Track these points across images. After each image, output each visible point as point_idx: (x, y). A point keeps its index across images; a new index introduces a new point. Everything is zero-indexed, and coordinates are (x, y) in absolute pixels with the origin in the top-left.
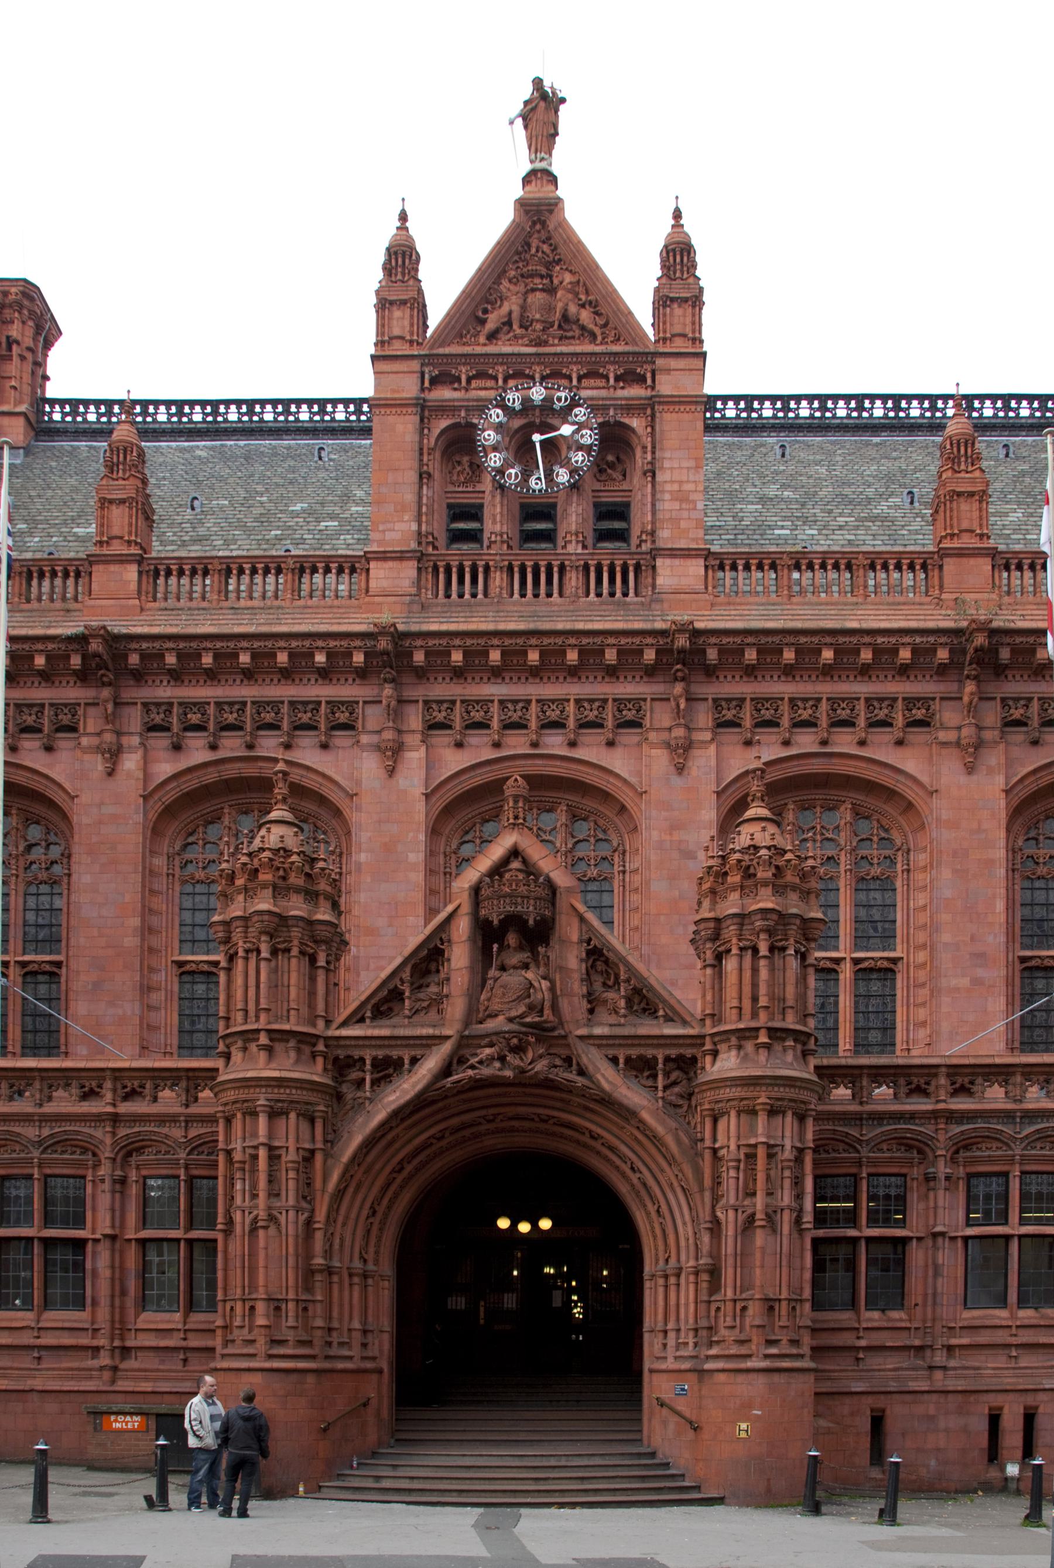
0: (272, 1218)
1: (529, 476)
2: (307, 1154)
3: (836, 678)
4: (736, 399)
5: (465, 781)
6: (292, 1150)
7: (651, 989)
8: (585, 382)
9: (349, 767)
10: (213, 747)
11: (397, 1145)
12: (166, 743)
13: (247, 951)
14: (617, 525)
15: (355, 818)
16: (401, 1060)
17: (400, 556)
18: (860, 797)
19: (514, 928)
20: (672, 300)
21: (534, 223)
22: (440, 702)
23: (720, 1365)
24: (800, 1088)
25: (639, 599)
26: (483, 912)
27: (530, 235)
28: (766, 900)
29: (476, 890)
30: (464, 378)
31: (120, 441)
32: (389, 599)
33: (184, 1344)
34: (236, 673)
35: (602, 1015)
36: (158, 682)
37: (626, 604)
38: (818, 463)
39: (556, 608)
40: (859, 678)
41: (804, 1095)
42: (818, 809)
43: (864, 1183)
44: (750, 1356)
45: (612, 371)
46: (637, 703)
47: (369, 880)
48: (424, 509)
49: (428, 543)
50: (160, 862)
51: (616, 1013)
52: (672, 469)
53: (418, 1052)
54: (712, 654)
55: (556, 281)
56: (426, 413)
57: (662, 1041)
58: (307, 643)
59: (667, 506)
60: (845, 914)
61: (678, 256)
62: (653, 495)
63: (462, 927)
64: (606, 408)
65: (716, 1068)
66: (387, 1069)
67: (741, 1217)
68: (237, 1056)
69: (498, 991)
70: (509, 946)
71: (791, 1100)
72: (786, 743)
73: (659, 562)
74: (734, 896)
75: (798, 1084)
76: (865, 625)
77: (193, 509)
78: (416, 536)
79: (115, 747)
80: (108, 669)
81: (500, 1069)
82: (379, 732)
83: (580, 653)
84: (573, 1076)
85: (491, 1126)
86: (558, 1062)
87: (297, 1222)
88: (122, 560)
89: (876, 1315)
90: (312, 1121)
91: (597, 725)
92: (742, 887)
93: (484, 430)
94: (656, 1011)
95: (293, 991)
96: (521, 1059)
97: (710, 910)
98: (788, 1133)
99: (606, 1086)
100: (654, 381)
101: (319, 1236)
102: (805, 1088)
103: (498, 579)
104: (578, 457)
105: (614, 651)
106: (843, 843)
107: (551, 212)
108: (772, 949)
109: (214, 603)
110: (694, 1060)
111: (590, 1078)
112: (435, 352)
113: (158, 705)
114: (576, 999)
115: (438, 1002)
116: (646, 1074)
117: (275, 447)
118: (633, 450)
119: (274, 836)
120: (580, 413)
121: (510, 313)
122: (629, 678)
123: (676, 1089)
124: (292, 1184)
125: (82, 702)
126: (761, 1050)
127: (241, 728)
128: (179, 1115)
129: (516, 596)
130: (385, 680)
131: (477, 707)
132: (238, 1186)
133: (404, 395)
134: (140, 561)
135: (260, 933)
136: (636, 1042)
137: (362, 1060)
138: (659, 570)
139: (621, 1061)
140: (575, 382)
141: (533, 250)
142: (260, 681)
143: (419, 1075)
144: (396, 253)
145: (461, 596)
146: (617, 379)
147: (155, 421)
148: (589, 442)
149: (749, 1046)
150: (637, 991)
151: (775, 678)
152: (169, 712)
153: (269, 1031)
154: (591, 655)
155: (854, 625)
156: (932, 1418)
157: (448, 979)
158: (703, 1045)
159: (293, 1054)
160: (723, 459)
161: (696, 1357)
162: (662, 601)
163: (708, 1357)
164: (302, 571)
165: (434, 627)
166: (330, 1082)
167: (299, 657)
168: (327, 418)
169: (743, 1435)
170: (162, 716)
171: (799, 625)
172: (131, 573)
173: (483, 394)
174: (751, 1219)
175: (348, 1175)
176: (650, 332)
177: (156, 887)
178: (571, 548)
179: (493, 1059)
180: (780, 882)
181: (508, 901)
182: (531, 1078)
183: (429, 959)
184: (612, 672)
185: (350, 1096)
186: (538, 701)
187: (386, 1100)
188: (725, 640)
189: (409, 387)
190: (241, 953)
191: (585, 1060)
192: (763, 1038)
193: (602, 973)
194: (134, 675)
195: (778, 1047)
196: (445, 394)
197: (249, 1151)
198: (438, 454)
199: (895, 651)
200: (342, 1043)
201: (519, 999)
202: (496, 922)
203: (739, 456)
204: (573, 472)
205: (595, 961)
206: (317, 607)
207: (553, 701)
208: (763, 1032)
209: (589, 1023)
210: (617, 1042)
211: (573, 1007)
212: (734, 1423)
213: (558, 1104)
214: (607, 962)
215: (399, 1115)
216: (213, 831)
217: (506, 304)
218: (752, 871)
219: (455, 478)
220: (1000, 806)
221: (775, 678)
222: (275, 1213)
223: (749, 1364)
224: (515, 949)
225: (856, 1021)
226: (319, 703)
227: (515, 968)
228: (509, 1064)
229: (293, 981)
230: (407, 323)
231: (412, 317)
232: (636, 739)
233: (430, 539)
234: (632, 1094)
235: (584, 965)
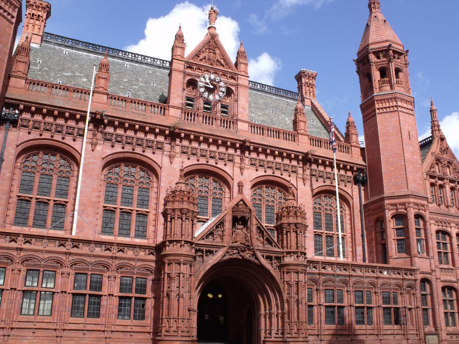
12: (110, 144)
17: (178, 108)
23: (292, 340)
43: (135, 280)
53: (217, 249)
63: (229, 218)
73: (238, 122)
115: (222, 237)
137: (203, 250)
163: (287, 337)
208: (299, 253)
211: (254, 241)
223: (299, 340)
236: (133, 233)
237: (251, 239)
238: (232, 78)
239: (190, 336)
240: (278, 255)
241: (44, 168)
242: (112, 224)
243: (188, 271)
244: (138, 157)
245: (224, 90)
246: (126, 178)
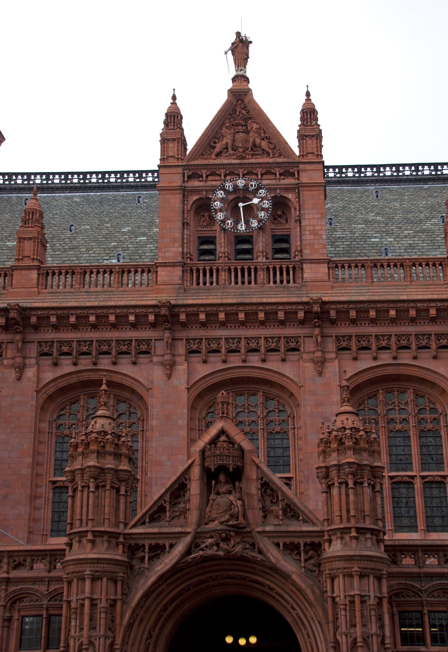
0: (91, 643)
1: (237, 224)
2: (112, 602)
3: (398, 324)
4: (353, 167)
5: (208, 381)
6: (104, 600)
7: (295, 505)
8: (265, 177)
9: (146, 374)
10: (75, 364)
11: (163, 595)
13: (83, 487)
14: (284, 246)
15: (150, 401)
17: (173, 265)
18: (417, 386)
19: (223, 473)
20: (306, 136)
21: (238, 100)
22: (194, 339)
24: (376, 561)
25: (295, 285)
26: (206, 464)
27: (236, 106)
28: (350, 458)
29: (203, 452)
30: (204, 176)
31: (30, 209)
32: (166, 289)
34: (88, 326)
35: (271, 519)
36: (46, 331)
37: (288, 287)
38: (395, 200)
39: (253, 290)
40: (410, 324)
41: (379, 566)
42: (396, 392)
45: (278, 171)
46: (296, 338)
47: (157, 435)
48: (185, 241)
49: (187, 258)
50: (45, 426)
51: (278, 518)
52: (309, 219)
53: (173, 541)
54: (333, 314)
55: (249, 128)
56: (186, 193)
57: (302, 534)
58: (125, 311)
59: (308, 237)
60: (415, 450)
61: (309, 114)
62: (300, 232)
63: (196, 472)
64: (275, 189)
65: (331, 550)
66: (157, 551)
68: (75, 545)
69: (215, 507)
70: (221, 481)
71: (371, 569)
72: (375, 359)
73: (305, 266)
74: (335, 455)
75: (375, 559)
76: (410, 298)
77: (71, 231)
78: (181, 255)
79: (22, 365)
80: (19, 325)
81: (217, 551)
82: (162, 355)
83: (265, 314)
84: (255, 554)
86: (248, 546)
87: (105, 645)
88: (29, 268)
91: (276, 350)
92: (338, 450)
93: (215, 201)
94: (299, 517)
95: (107, 509)
96: (228, 545)
97: (323, 462)
98: (371, 589)
99: (273, 560)
100: (298, 175)
102: (378, 562)
103: (223, 276)
104: (262, 214)
105: (283, 313)
106: (410, 411)
107: (246, 95)
108: (355, 483)
109: (77, 289)
110: (320, 544)
111: (264, 555)
112: (189, 163)
113: (46, 342)
114: (256, 511)
115: (184, 512)
116: (295, 552)
117: (115, 196)
119: (99, 424)
120: (262, 192)
121: (227, 143)
122: (292, 326)
123: (312, 561)
124: (103, 621)
125: (5, 341)
126: (353, 540)
127: (90, 354)
129: (233, 284)
130: (166, 329)
131: (214, 342)
132: (73, 623)
133: (175, 185)
134: (39, 268)
135: (90, 477)
136: (288, 535)
137: (144, 546)
138: (305, 270)
139: (281, 545)
140: (259, 177)
141: (238, 113)
142: (100, 330)
143: (174, 555)
144: (170, 116)
145: (205, 284)
146: (281, 175)
147: (53, 183)
148: (267, 207)
149: (347, 538)
150: (288, 506)
151: (367, 325)
152: (52, 346)
153: (93, 532)
154: (271, 315)
155: (405, 297)
157: (189, 500)
158: (324, 536)
159: (106, 544)
160: (346, 199)
162: (307, 286)
164: (123, 272)
165: (190, 302)
166: (126, 559)
167: (121, 317)
168: (143, 180)
170: (48, 348)
171: (376, 298)
172: (34, 274)
173: (214, 183)
175: (135, 614)
176: (297, 151)
177: (42, 439)
178: (260, 259)
179: (213, 545)
180: (357, 447)
182: (233, 555)
183: (179, 489)
184: (282, 323)
185: (137, 567)
186: (245, 338)
188: (339, 306)
189: (177, 181)
191: (261, 545)
192: (354, 534)
193: (270, 495)
194: (33, 327)
195: (362, 538)
196: (196, 183)
197: (80, 602)
198: (192, 213)
199: (428, 310)
200: (133, 536)
201: (226, 511)
202: (213, 470)
203: (355, 197)
204: (259, 221)
205: (266, 489)
206: (131, 291)
207: (253, 338)
208: (353, 531)
209: (264, 524)
210: (278, 534)
211: (255, 515)
213: (250, 570)
214: (272, 489)
215: (163, 578)
216: (75, 407)
217: (225, 139)
218: (343, 441)
219: (201, 224)
221: (367, 325)
222: (93, 639)
224: (224, 483)
225: (426, 512)
226: (131, 341)
227: (224, 493)
228: (222, 548)
229: (107, 503)
230: (176, 149)
231: (178, 146)
232: (297, 357)
233: (189, 256)
234: (287, 564)
235: (260, 492)
236: (421, 525)
238: (286, 174)
241: (242, 422)
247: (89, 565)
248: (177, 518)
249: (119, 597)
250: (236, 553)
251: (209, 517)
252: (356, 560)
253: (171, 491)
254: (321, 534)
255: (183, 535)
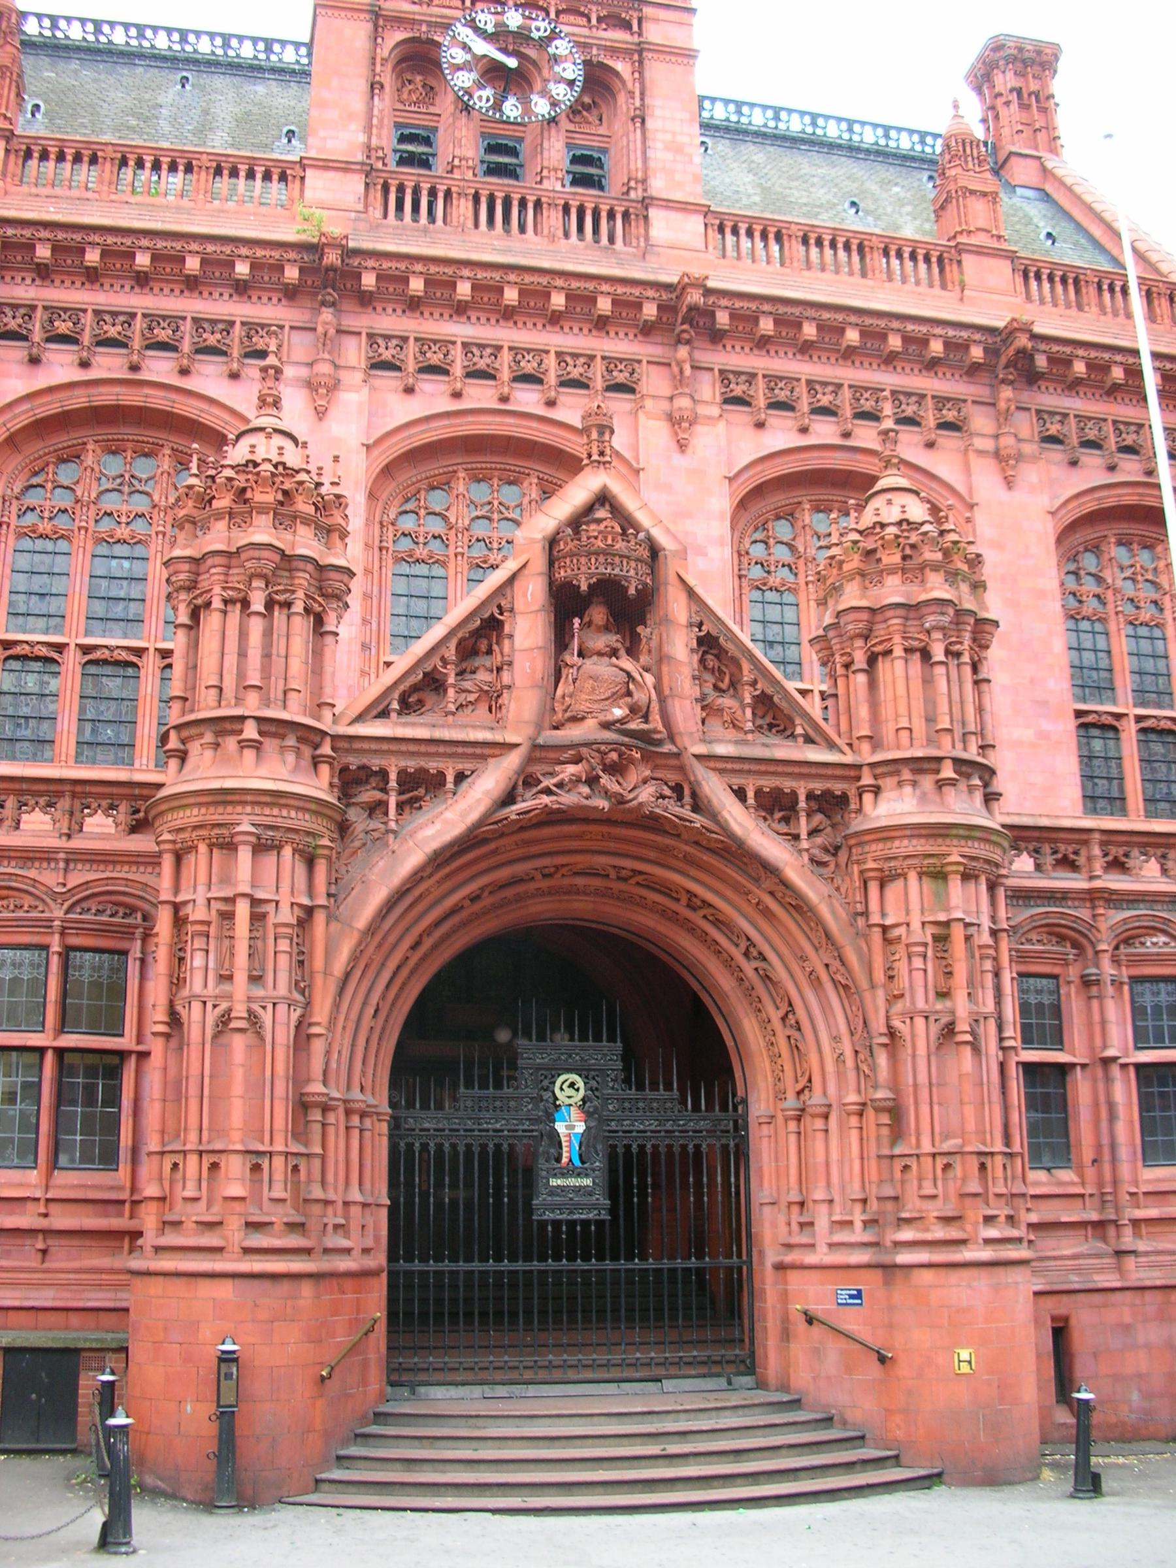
2: (302, 915)
10: (85, 364)
12: (23, 354)
16: (442, 775)
17: (345, 167)
22: (388, 338)
23: (923, 1256)
29: (552, 542)
33: (43, 1223)
44: (963, 1242)
46: (632, 363)
48: (375, 121)
49: (378, 158)
53: (466, 766)
56: (381, 22)
57: (805, 770)
63: (532, 593)
64: (590, 46)
66: (421, 787)
67: (935, 1029)
72: (804, 430)
73: (653, 213)
85: (545, 884)
86: (667, 792)
89: (1041, 1175)
90: (310, 862)
101: (318, 1046)
105: (609, 301)
110: (843, 800)
111: (714, 816)
115: (493, 699)
118: (614, 96)
123: (819, 840)
128: (56, 850)
136: (772, 768)
137: (383, 774)
139: (750, 794)
146: (599, 20)
153: (259, 719)
154: (581, 303)
156: (1127, 1328)
161: (876, 1244)
163: (897, 1244)
169: (965, 1368)
174: (949, 1031)
179: (579, 780)
181: (601, 559)
182: (630, 811)
187: (420, 835)
190: (217, 603)
193: (712, 671)
198: (389, 66)
200: (357, 745)
201: (614, 698)
205: (705, 653)
210: (746, 767)
211: (685, 714)
212: (950, 1350)
213: (652, 855)
219: (405, 96)
220: (1048, 529)
222: (255, 1007)
223: (968, 1254)
227: (600, 654)
232: (628, 406)
233: (380, 154)
237: (662, 700)
239: (308, 1251)
240: (828, 785)
242: (45, 725)
243: (285, 886)
244: (158, 400)
245: (571, 70)
246: (108, 507)
247: (248, 809)
248: (471, 707)
249: (322, 900)
250: (641, 804)
251: (565, 711)
252: (957, 836)
253: (460, 635)
254: (853, 773)
255: (497, 752)
